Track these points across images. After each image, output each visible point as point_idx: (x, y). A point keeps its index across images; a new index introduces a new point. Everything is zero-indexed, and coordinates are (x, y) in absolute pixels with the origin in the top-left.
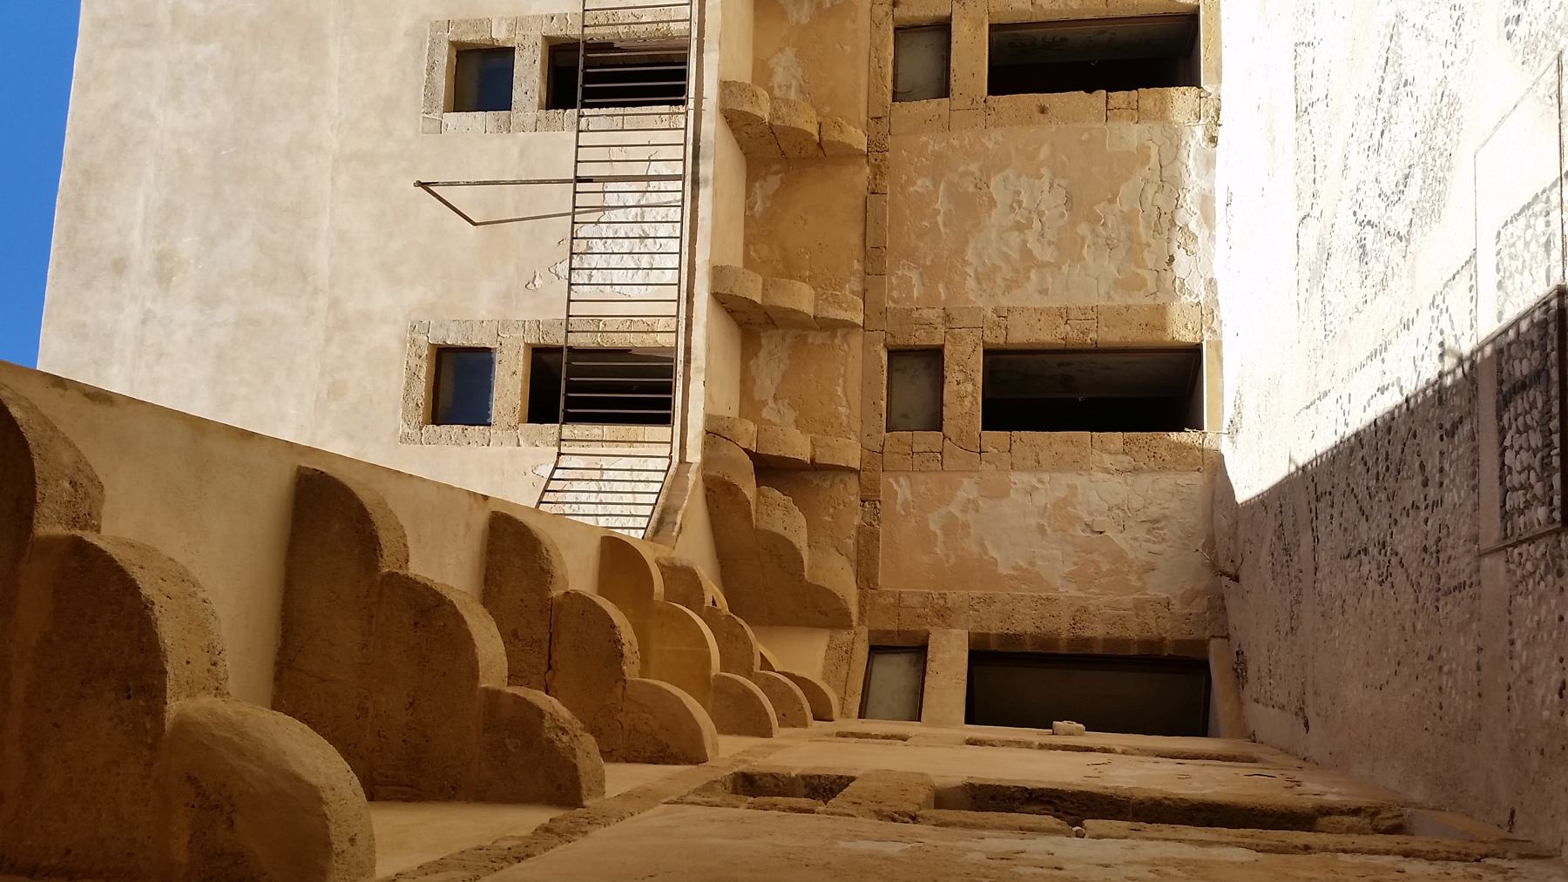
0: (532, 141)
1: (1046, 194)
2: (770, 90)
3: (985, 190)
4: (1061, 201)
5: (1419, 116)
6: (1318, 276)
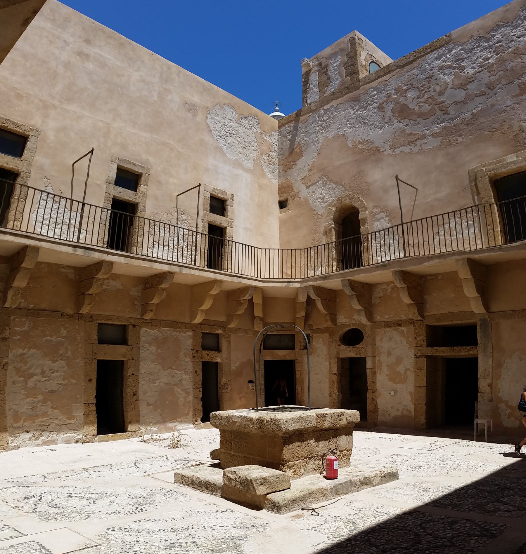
0: (101, 192)
1: (57, 382)
2: (108, 279)
5: (82, 507)
6: (19, 484)
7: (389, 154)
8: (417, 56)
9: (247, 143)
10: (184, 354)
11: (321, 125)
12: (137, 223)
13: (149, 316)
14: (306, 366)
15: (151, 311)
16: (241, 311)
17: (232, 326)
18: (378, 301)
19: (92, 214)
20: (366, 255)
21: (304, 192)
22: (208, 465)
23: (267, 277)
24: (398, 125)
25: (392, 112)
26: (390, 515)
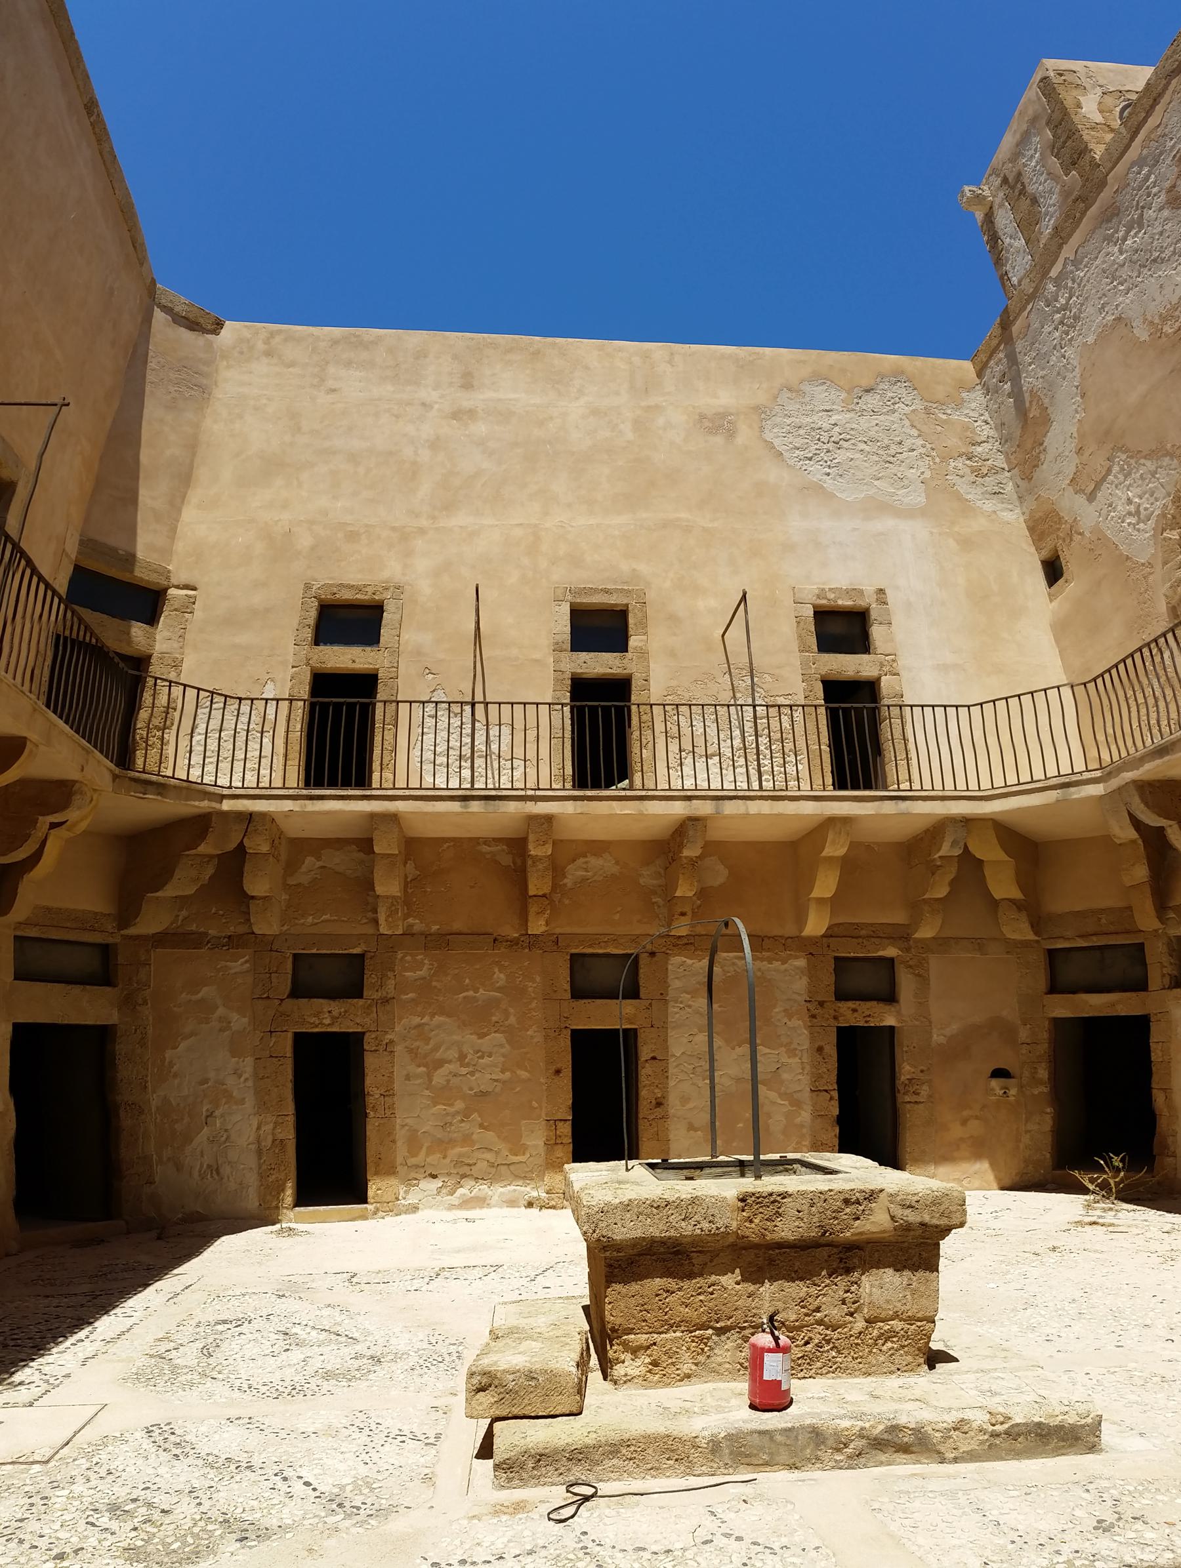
3: (493, 1029)
4: (483, 1088)
9: (893, 446)
10: (785, 1010)
11: (1061, 323)
17: (926, 932)
19: (531, 722)
21: (1086, 514)
23: (1012, 780)
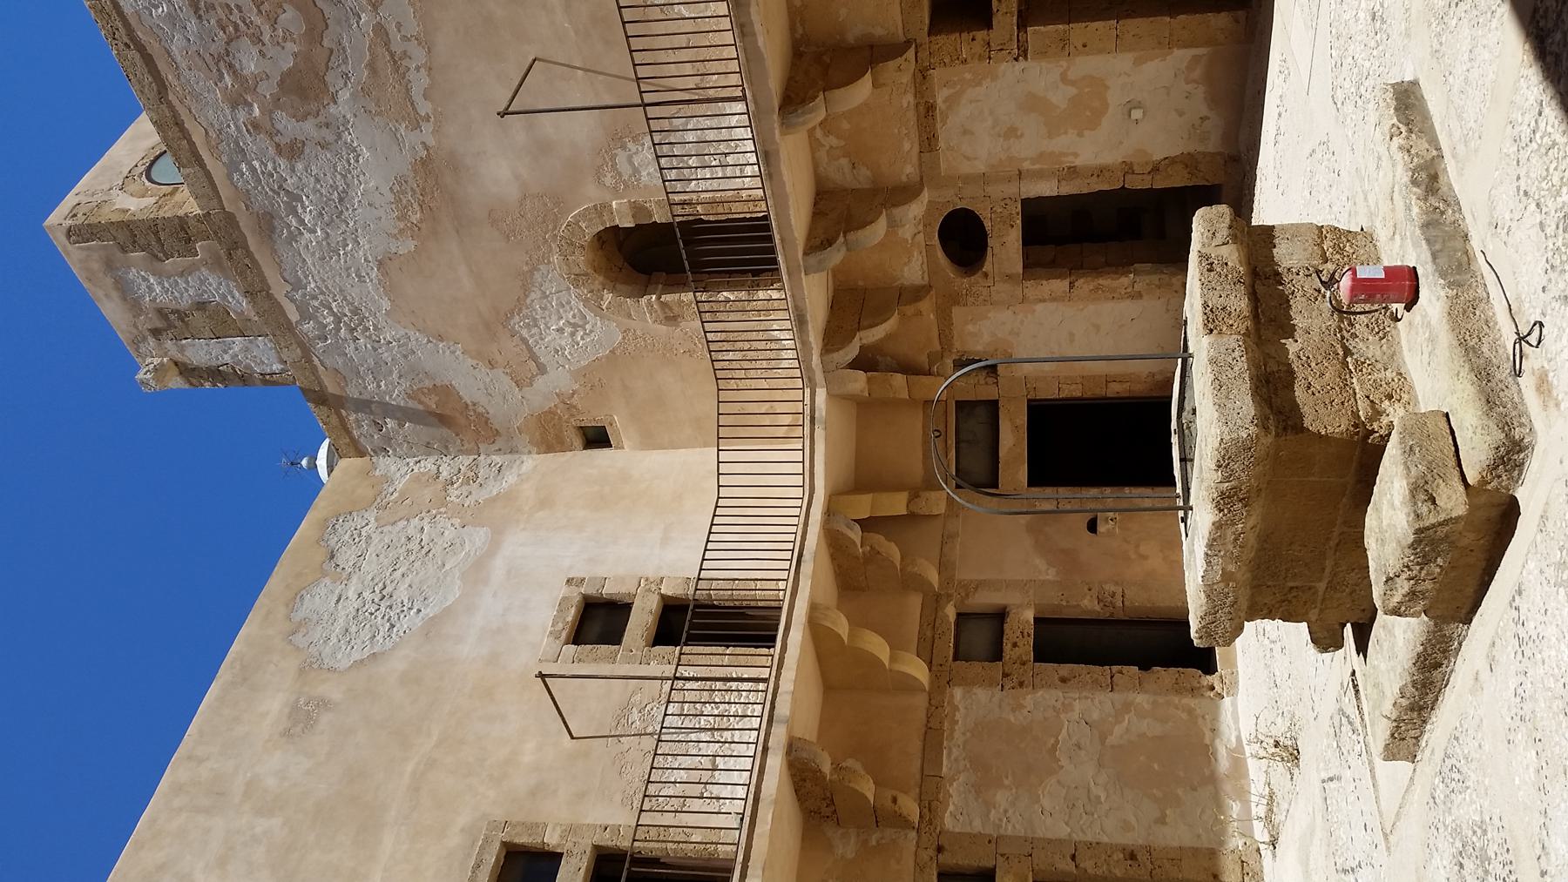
7: (436, 132)
8: (126, 40)
11: (352, 330)
12: (652, 845)
13: (910, 807)
14: (1047, 366)
15: (895, 800)
16: (893, 552)
17: (934, 577)
18: (864, 173)
20: (736, 207)
21: (557, 381)
22: (1356, 660)
24: (343, 104)
25: (304, 118)
26: (1546, 98)
